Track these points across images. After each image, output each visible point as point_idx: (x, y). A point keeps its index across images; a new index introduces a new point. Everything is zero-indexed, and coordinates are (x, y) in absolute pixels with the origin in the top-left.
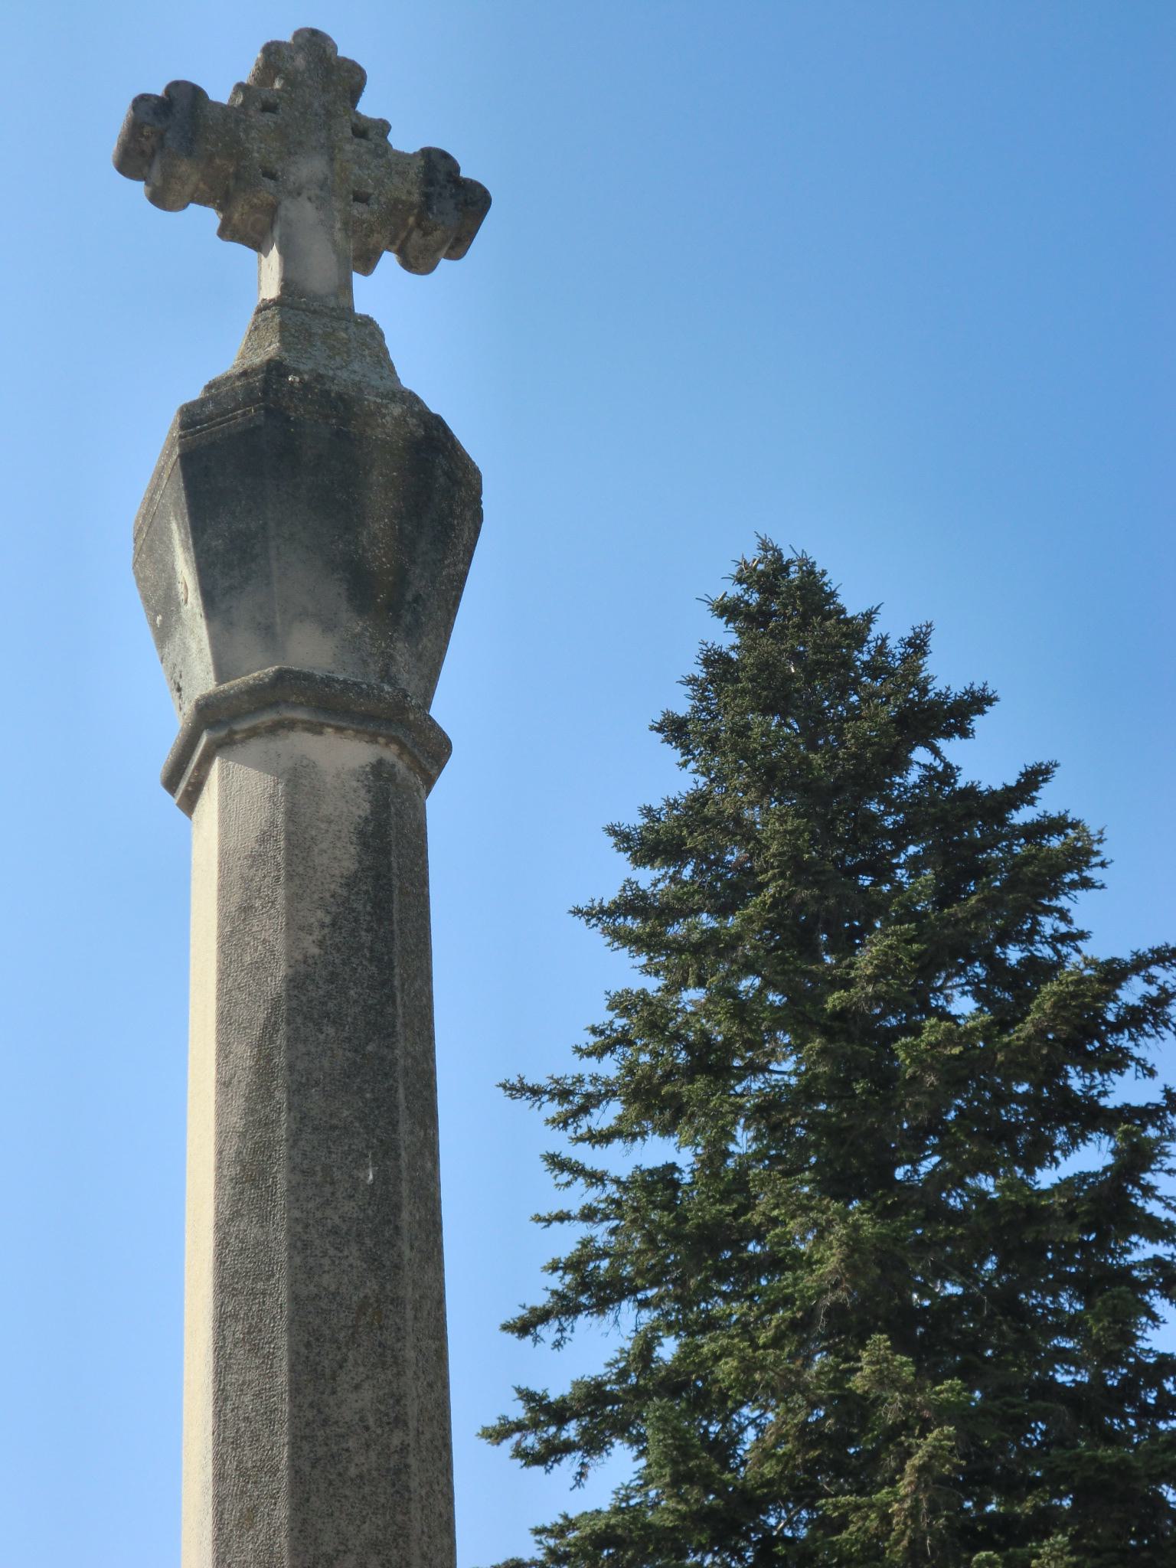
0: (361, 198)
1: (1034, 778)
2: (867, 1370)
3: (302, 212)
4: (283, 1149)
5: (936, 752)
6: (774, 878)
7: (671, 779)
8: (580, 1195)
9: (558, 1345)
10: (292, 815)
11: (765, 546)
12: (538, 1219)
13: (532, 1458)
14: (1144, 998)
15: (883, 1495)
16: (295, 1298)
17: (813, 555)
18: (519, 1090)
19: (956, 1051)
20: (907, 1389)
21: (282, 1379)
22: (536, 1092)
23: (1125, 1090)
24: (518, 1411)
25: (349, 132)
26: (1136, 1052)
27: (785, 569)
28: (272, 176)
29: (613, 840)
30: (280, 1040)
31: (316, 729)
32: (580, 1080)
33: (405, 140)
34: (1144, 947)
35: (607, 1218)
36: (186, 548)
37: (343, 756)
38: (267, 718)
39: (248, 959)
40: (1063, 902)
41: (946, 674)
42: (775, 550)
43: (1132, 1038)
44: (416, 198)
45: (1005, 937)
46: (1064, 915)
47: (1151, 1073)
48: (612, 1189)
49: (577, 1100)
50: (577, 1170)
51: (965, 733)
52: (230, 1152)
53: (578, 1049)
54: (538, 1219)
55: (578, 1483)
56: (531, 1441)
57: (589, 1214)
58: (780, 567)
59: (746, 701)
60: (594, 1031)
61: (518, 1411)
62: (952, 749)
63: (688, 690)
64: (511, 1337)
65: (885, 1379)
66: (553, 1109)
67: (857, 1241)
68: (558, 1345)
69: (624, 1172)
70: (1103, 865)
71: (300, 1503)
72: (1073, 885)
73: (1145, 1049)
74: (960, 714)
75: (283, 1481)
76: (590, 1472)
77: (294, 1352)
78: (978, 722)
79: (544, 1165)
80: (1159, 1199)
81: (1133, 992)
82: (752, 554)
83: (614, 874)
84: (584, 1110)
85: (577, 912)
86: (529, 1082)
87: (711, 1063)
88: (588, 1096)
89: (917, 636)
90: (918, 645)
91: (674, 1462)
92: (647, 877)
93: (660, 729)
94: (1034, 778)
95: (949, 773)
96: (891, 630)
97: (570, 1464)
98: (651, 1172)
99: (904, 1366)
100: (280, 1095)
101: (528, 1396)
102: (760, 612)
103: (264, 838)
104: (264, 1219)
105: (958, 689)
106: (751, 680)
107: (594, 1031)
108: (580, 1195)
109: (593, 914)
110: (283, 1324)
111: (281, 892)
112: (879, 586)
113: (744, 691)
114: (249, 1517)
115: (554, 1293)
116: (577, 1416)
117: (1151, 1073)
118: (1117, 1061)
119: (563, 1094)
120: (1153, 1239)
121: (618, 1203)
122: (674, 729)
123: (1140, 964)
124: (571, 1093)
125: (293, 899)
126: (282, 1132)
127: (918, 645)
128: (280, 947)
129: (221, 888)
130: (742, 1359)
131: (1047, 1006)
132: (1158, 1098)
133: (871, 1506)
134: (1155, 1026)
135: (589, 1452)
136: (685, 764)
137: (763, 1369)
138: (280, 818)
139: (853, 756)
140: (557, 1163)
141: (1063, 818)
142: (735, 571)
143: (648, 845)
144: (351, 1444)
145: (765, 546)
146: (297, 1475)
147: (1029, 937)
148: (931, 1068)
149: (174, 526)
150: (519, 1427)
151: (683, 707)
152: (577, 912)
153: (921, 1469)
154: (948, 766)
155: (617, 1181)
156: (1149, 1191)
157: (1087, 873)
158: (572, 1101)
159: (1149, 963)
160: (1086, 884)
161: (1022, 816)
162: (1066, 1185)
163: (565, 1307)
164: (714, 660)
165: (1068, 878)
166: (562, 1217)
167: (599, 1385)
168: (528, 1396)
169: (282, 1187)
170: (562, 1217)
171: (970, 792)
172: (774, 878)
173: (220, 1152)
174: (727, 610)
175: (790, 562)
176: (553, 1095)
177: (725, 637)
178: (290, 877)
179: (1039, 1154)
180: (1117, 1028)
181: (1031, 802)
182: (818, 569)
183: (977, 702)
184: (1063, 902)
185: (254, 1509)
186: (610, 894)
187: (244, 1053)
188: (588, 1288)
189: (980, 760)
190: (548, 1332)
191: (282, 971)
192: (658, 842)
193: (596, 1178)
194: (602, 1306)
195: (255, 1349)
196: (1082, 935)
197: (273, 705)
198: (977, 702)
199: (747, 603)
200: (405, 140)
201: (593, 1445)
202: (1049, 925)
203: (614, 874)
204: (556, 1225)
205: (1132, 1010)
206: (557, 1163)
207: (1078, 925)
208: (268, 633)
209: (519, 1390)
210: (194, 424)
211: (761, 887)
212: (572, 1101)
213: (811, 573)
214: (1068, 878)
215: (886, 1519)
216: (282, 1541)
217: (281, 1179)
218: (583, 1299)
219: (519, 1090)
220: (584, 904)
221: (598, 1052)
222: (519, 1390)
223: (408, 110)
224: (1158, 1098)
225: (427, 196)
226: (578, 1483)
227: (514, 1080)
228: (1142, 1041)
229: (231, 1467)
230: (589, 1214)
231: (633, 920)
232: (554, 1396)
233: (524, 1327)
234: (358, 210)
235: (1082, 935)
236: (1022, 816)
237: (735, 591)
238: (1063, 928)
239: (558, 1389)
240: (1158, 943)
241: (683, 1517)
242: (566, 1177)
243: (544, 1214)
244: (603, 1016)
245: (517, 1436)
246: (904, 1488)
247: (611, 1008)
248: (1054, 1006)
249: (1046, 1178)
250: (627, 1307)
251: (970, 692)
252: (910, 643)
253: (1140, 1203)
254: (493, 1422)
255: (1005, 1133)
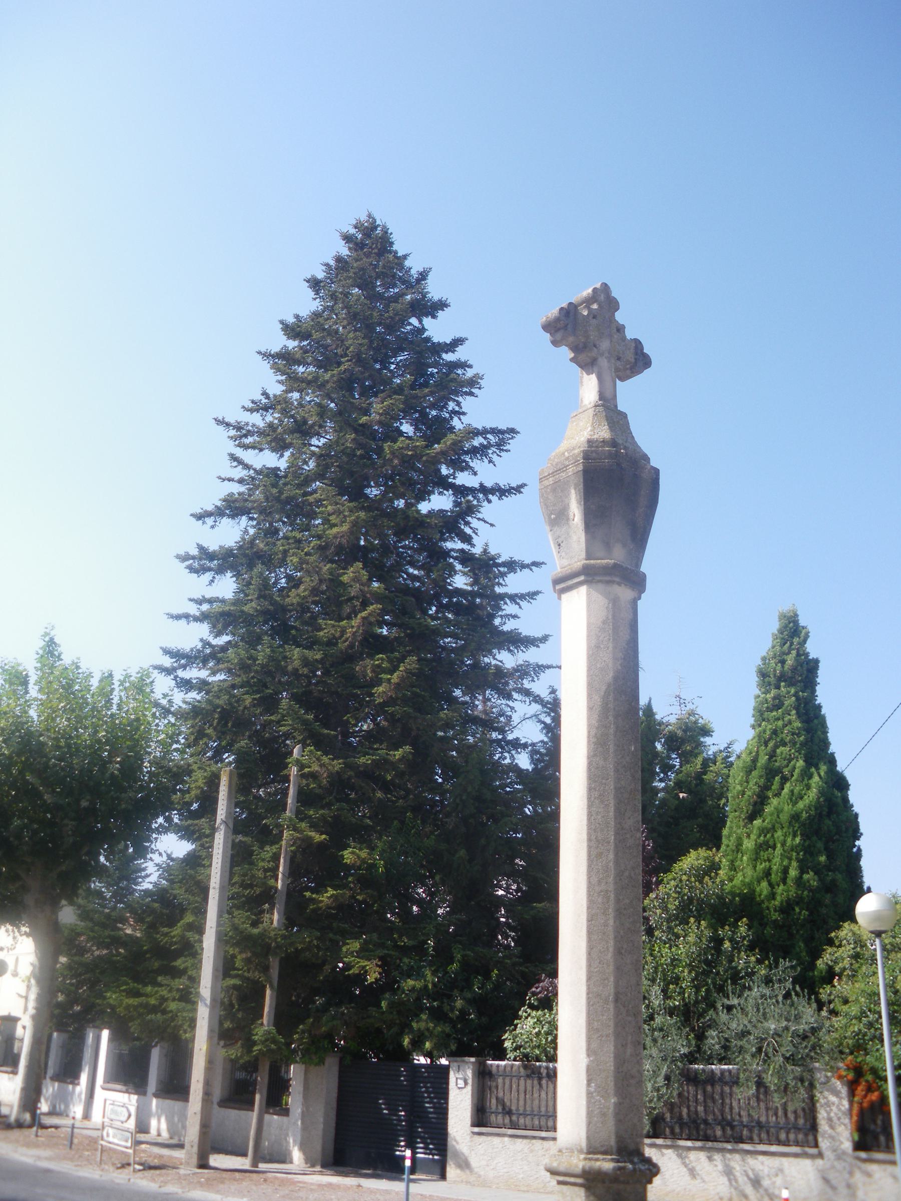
0: (619, 359)
1: (457, 343)
2: (351, 575)
3: (603, 362)
4: (612, 737)
5: (420, 322)
6: (348, 361)
7: (307, 304)
8: (239, 473)
9: (212, 527)
10: (614, 616)
11: (370, 216)
12: (219, 478)
13: (192, 569)
14: (480, 444)
15: (344, 623)
16: (615, 788)
17: (389, 225)
18: (220, 422)
19: (410, 453)
20: (362, 584)
21: (612, 814)
22: (228, 425)
23: (463, 479)
24: (195, 552)
25: (615, 330)
26: (471, 464)
27: (376, 228)
28: (595, 346)
29: (281, 326)
30: (611, 698)
31: (619, 584)
32: (247, 424)
33: (630, 334)
34: (488, 426)
35: (248, 484)
36: (579, 503)
37: (625, 593)
38: (608, 578)
39: (599, 666)
40: (460, 399)
41: (434, 290)
42: (373, 218)
43: (471, 458)
44: (633, 360)
45: (433, 406)
46: (458, 404)
47: (475, 474)
48: (252, 472)
49: (244, 432)
50: (239, 461)
51: (434, 317)
52: (593, 733)
53: (243, 407)
54: (219, 478)
55: (210, 584)
56: (196, 565)
57: (241, 481)
58: (374, 227)
59: (350, 281)
60: (253, 402)
61: (195, 552)
62: (427, 322)
63: (324, 268)
64: (193, 520)
65: (356, 579)
66: (233, 432)
67: (357, 522)
68: (212, 527)
69: (258, 466)
70: (480, 388)
71: (616, 855)
72: (467, 394)
73: (475, 464)
74: (433, 308)
75: (612, 847)
76: (216, 581)
77: (615, 805)
78: (440, 314)
79: (228, 457)
80: (471, 528)
81: (477, 441)
82: (363, 217)
83: (280, 342)
84: (246, 436)
85: (259, 353)
86: (226, 420)
87: (303, 430)
88: (249, 431)
89: (424, 271)
90: (423, 276)
91: (260, 590)
92: (292, 344)
93: (308, 281)
94: (457, 343)
95: (423, 330)
96: (414, 265)
97: (208, 576)
98: (268, 468)
99: (364, 575)
100: (611, 718)
101: (201, 548)
102: (361, 243)
103: (604, 622)
104: (605, 759)
105: (436, 298)
106: (354, 273)
107: (253, 402)
108: (239, 473)
109: (266, 355)
110: (612, 796)
111: (611, 645)
112: (413, 247)
113: (350, 277)
114: (599, 855)
115: (216, 506)
116: (218, 560)
117: (475, 474)
118: (467, 468)
119: (238, 428)
120: (463, 542)
121: (253, 478)
122: (315, 284)
123: (484, 432)
124: (243, 428)
125: (615, 648)
126: (612, 731)
127: (423, 276)
128: (610, 665)
129: (588, 636)
130: (300, 559)
131: (448, 443)
132: (477, 486)
133: (339, 626)
134: (481, 455)
135: (217, 573)
136: (315, 299)
137: (308, 563)
138: (610, 617)
139: (391, 317)
140: (233, 458)
141: (466, 362)
142: (354, 222)
143: (292, 330)
144: (628, 836)
145: (370, 216)
146: (616, 846)
147: (441, 409)
148: (397, 456)
149: (573, 491)
150: (193, 558)
151: (321, 275)
152: (259, 353)
153: (363, 618)
154: (423, 328)
155: (255, 470)
156: (467, 523)
157: (473, 390)
158: (241, 432)
159: (489, 433)
160: (471, 394)
161: (448, 357)
162: (431, 513)
163: (219, 513)
164: (339, 259)
165: (465, 390)
166: (230, 480)
167: (232, 550)
168: (201, 548)
169: (611, 750)
170: (230, 480)
171: (428, 339)
172: (348, 361)
173: (589, 732)
174: (347, 238)
175: (379, 225)
176: (234, 427)
177: (344, 250)
178: (614, 639)
179: (423, 496)
180: (467, 453)
181: (453, 352)
182: (389, 231)
183: (442, 305)
184: (460, 399)
185: (602, 853)
186: (276, 348)
187: (597, 699)
188: (233, 508)
189: (437, 329)
190: (210, 521)
191: (611, 674)
192: (300, 332)
193: (247, 467)
194: (233, 516)
195: (602, 802)
196: (464, 414)
197: (610, 574)
198: (442, 305)
199: (356, 238)
200: (630, 334)
201: (220, 571)
202: (451, 405)
203: (280, 342)
204: (226, 482)
205: (475, 448)
206: (233, 458)
207: (463, 410)
208: (608, 546)
209: (198, 544)
210: (589, 459)
211: (339, 364)
212: (241, 432)
213: (386, 233)
214: (465, 390)
215: (343, 632)
216: (611, 864)
217: (612, 748)
218: (227, 512)
219: (220, 422)
220: (263, 350)
221: (251, 411)
222: (198, 544)
223: (633, 321)
224: (477, 486)
225: (636, 359)
226: (210, 584)
227: (220, 418)
228: (475, 460)
229: (593, 837)
230: (241, 481)
231: (283, 361)
232: (211, 549)
233: (200, 517)
234: (618, 363)
235: (464, 414)
236: (448, 357)
237: (353, 231)
238: (457, 409)
239: (213, 547)
240: (494, 426)
241: (257, 611)
242: (235, 464)
243: (223, 476)
244: (258, 397)
245: (191, 561)
246: (355, 622)
247: (262, 394)
248: (452, 444)
249: (424, 507)
250: (244, 518)
251: (440, 301)
252: (421, 274)
253: (462, 527)
254: (182, 553)
255: (411, 483)
